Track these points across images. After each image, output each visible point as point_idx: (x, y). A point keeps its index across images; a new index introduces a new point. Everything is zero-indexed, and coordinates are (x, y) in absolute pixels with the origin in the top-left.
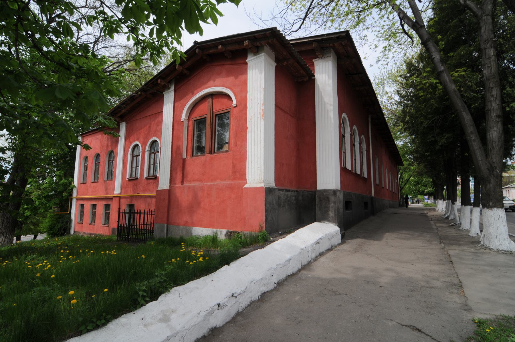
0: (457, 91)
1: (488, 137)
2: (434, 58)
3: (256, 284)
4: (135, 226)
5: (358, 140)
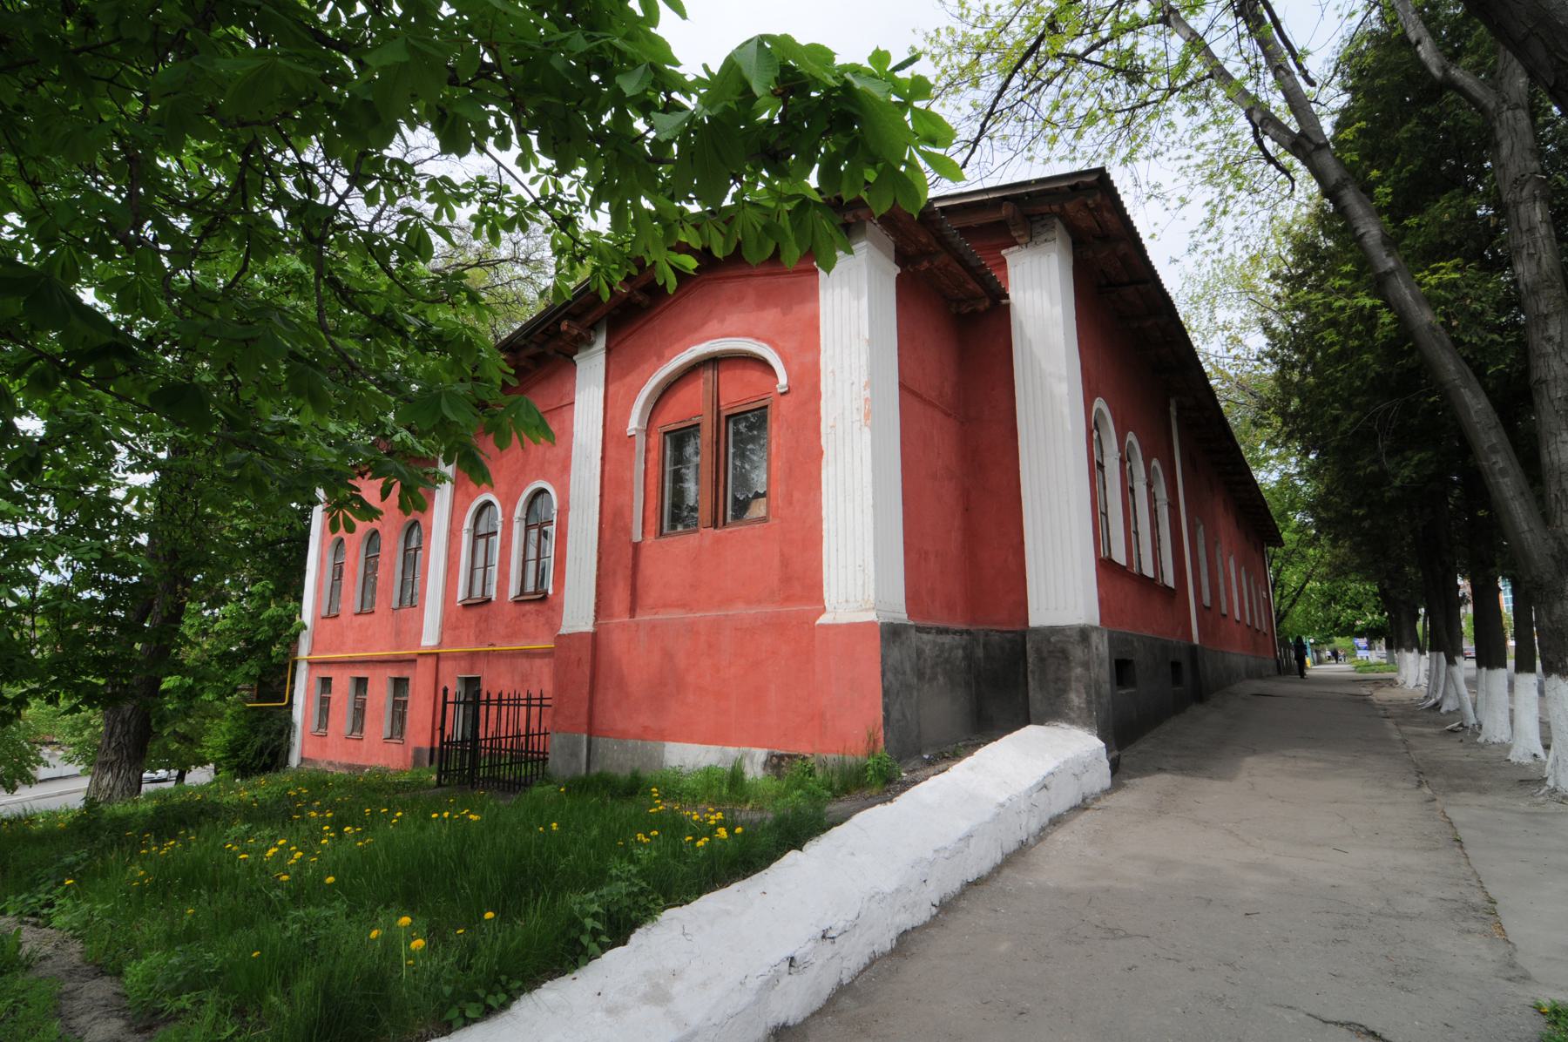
0: (1439, 327)
1: (1546, 459)
2: (1363, 234)
3: (883, 905)
4: (503, 741)
5: (1144, 475)
